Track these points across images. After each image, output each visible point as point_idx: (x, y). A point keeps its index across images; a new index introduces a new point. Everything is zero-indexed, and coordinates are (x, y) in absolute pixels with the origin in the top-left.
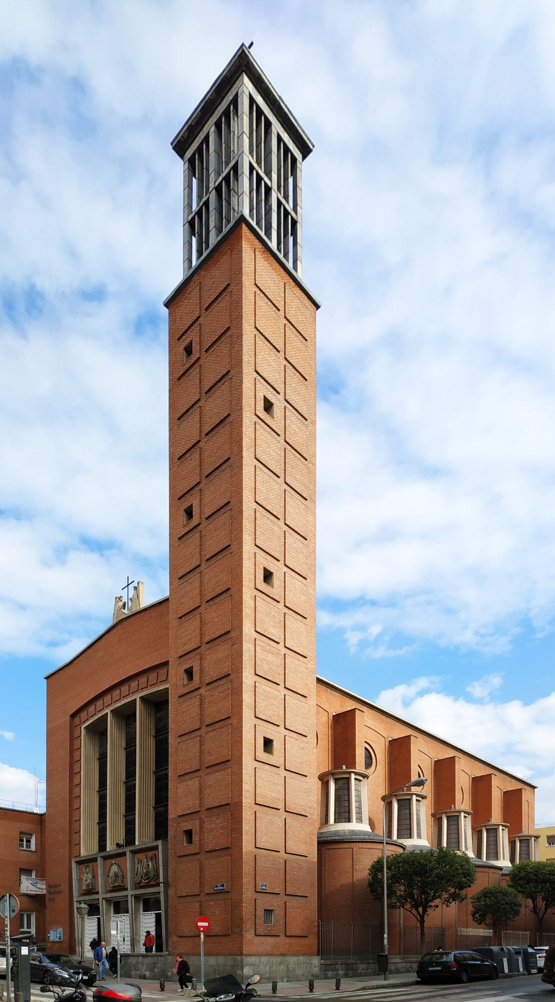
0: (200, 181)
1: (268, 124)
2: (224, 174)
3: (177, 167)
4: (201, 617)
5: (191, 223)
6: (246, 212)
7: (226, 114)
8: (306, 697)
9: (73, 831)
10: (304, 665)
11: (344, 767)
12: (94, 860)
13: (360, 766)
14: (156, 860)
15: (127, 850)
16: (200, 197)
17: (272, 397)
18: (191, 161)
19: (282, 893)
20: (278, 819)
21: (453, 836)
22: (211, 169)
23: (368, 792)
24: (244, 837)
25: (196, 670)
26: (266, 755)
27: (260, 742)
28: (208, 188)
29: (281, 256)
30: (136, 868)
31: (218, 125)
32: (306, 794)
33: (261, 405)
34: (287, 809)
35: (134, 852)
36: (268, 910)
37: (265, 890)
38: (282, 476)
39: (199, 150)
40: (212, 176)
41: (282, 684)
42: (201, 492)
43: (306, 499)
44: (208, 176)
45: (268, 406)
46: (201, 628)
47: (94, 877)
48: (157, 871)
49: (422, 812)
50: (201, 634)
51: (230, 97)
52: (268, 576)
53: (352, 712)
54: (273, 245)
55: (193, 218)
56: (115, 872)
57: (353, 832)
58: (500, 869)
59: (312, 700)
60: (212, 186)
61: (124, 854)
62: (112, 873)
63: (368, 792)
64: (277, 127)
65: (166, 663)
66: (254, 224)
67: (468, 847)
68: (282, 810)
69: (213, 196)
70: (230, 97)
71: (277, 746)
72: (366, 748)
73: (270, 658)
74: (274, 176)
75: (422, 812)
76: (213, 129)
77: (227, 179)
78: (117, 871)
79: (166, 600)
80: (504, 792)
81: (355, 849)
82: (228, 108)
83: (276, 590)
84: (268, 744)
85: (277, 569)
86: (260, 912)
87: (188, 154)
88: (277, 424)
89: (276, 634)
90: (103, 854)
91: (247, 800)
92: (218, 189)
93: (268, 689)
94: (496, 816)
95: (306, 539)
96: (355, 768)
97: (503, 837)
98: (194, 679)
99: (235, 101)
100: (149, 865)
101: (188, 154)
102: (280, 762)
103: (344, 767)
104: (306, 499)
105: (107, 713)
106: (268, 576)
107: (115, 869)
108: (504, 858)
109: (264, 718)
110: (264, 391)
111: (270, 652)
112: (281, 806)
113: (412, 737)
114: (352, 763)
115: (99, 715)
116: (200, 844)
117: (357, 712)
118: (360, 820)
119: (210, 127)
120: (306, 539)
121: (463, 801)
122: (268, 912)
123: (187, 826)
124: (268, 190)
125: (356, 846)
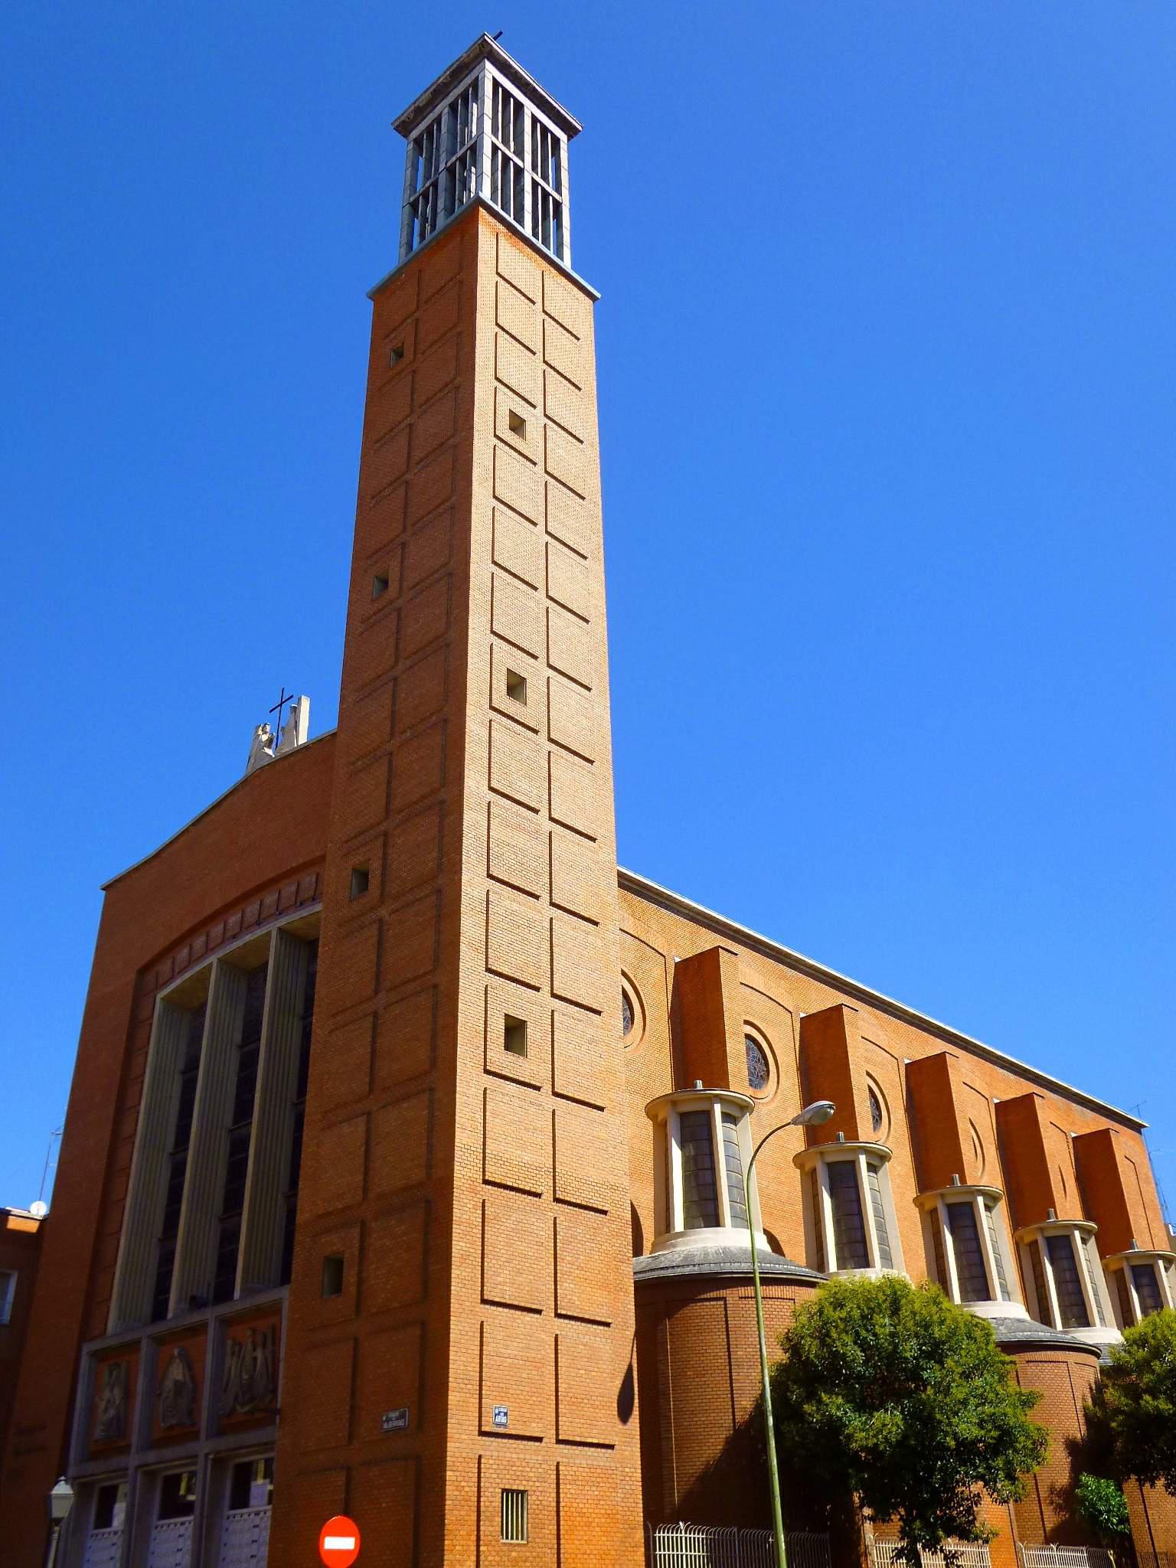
0: (429, 161)
1: (519, 106)
2: (459, 154)
3: (404, 147)
4: (390, 763)
5: (414, 206)
6: (486, 194)
7: (464, 96)
8: (596, 924)
9: (99, 1264)
10: (590, 854)
11: (699, 1084)
12: (133, 1346)
13: (739, 1084)
14: (274, 1343)
15: (210, 1315)
16: (427, 177)
17: (523, 410)
18: (418, 142)
19: (550, 1435)
20: (539, 1217)
21: (1065, 1264)
22: (443, 149)
23: (761, 1142)
24: (455, 1273)
25: (375, 866)
26: (510, 1057)
27: (498, 1027)
28: (437, 169)
29: (539, 243)
30: (227, 1366)
31: (453, 107)
32: (614, 1153)
33: (504, 422)
34: (559, 1195)
35: (226, 1322)
36: (513, 1491)
37: (505, 1425)
38: (541, 522)
39: (429, 130)
40: (443, 157)
41: (545, 897)
42: (403, 548)
43: (585, 558)
44: (438, 156)
45: (517, 425)
46: (389, 783)
47: (128, 1395)
48: (273, 1378)
49: (890, 1195)
50: (388, 795)
51: (468, 80)
52: (516, 686)
53: (713, 955)
54: (527, 230)
55: (417, 199)
56: (176, 1382)
57: (727, 1255)
58: (1093, 1351)
59: (610, 930)
60: (442, 167)
61: (198, 1329)
62: (169, 1384)
63: (761, 1142)
64: (530, 108)
65: (323, 858)
66: (498, 208)
67: (1010, 1289)
68: (548, 1196)
69: (443, 179)
70: (468, 80)
71: (535, 1034)
72: (748, 1037)
73: (521, 840)
74: (528, 157)
75: (890, 1195)
76: (446, 110)
77: (462, 160)
78: (180, 1377)
79: (334, 735)
80: (1074, 1139)
81: (730, 1300)
82: (466, 90)
83: (531, 711)
84: (515, 1033)
85: (535, 673)
86: (492, 1500)
87: (414, 134)
88: (535, 451)
89: (534, 794)
90: (160, 1328)
91: (465, 1172)
92: (451, 171)
93: (515, 907)
94: (1068, 1206)
95: (587, 621)
96: (727, 1087)
97: (1088, 1257)
98: (371, 887)
99: (476, 85)
100: (255, 1359)
101: (414, 134)
102: (542, 1077)
103: (699, 1084)
104: (585, 558)
105: (211, 964)
106: (516, 686)
107: (177, 1372)
108: (1102, 1319)
109: (506, 971)
110: (508, 402)
111: (519, 828)
112: (544, 1187)
113: (845, 1009)
114: (719, 1077)
115: (197, 968)
116: (359, 1292)
117: (723, 956)
118: (744, 1220)
119: (443, 107)
120: (587, 621)
121: (983, 1169)
122: (514, 1497)
123: (333, 1243)
124: (519, 172)
125: (732, 1295)
